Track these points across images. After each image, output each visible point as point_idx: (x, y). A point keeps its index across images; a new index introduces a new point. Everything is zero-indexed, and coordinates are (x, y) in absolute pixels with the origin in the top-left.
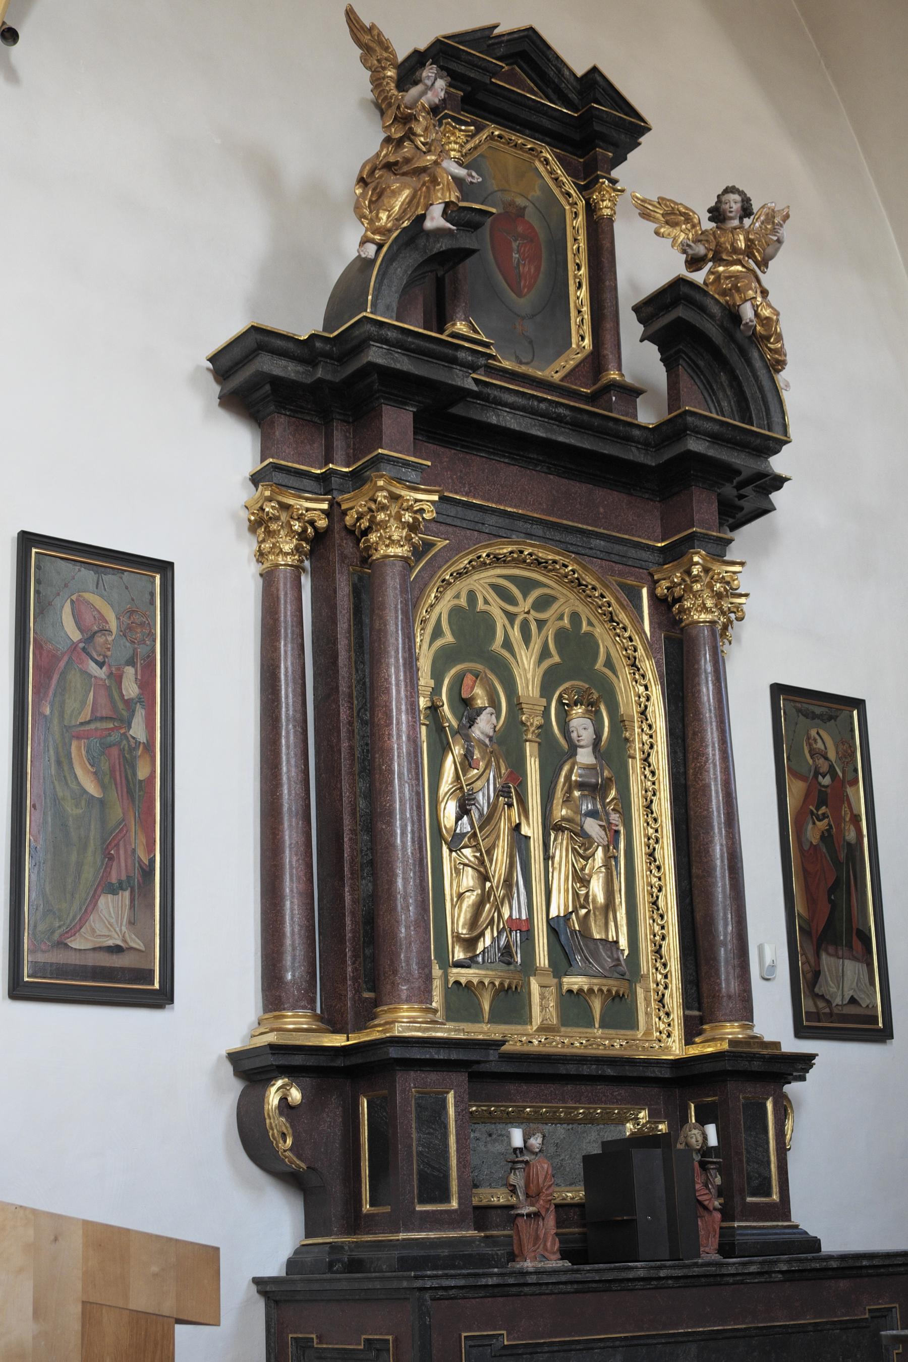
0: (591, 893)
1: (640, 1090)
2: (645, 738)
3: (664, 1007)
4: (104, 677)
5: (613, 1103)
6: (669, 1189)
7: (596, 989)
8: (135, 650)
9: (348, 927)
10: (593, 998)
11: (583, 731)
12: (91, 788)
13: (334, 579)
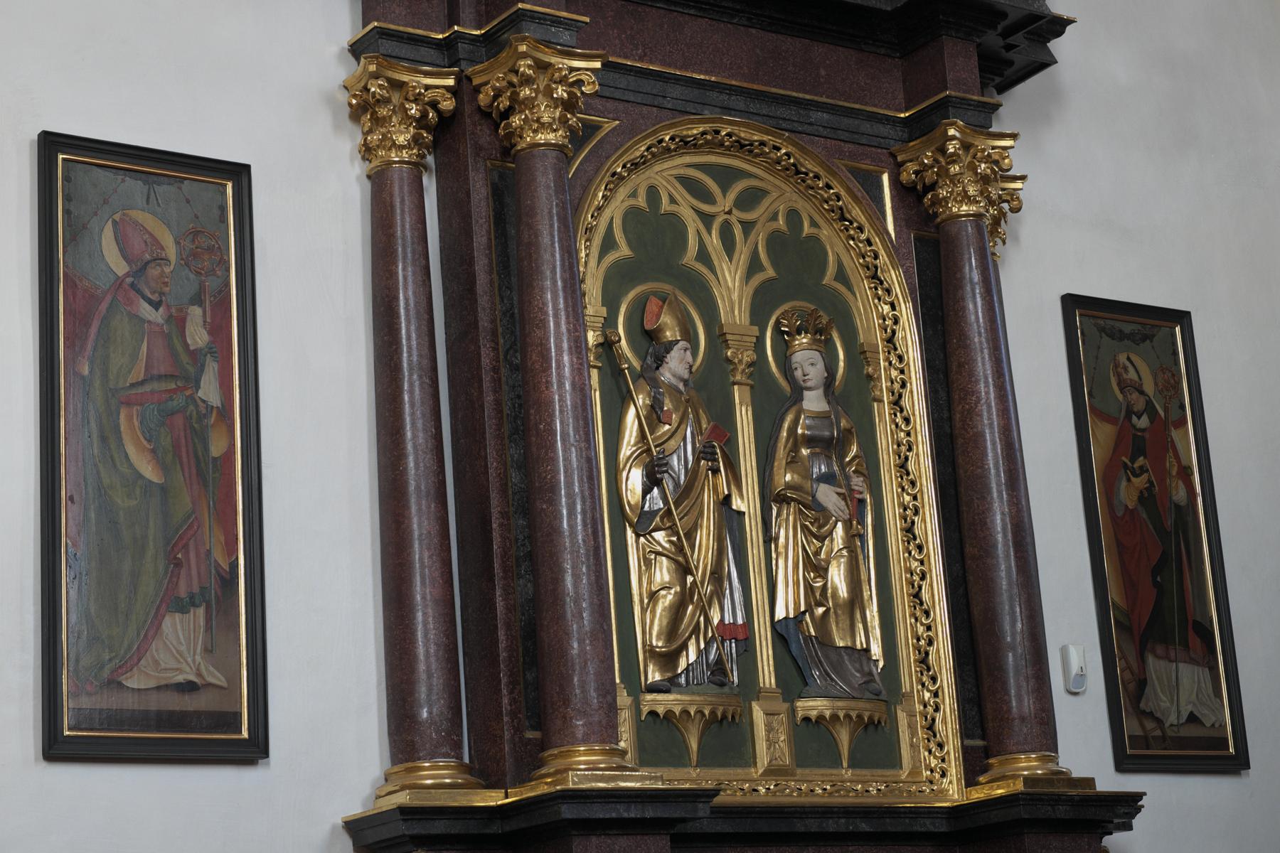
2: (894, 373)
3: (935, 736)
4: (160, 321)
9: (502, 645)
10: (838, 727)
12: (148, 471)
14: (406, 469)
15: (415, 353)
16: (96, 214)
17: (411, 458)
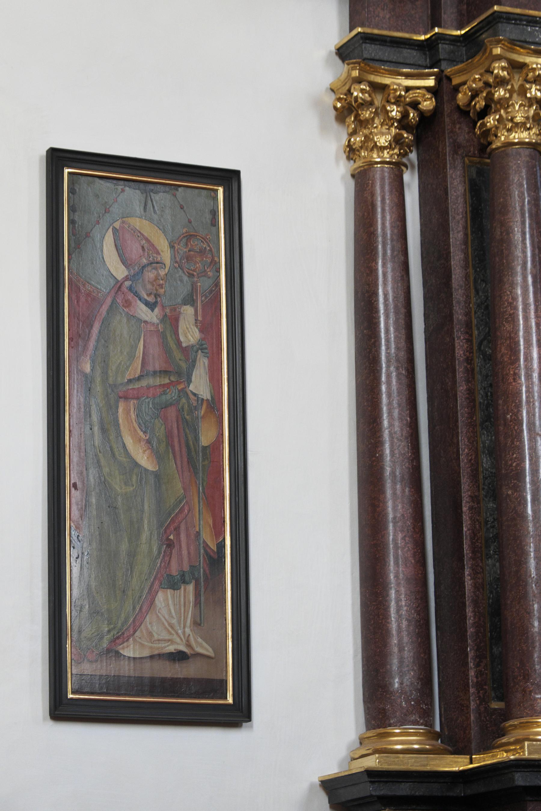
4: (155, 320)
8: (194, 287)
9: (470, 621)
12: (144, 460)
13: (445, 177)
14: (382, 456)
15: (393, 346)
16: (98, 223)
17: (387, 446)
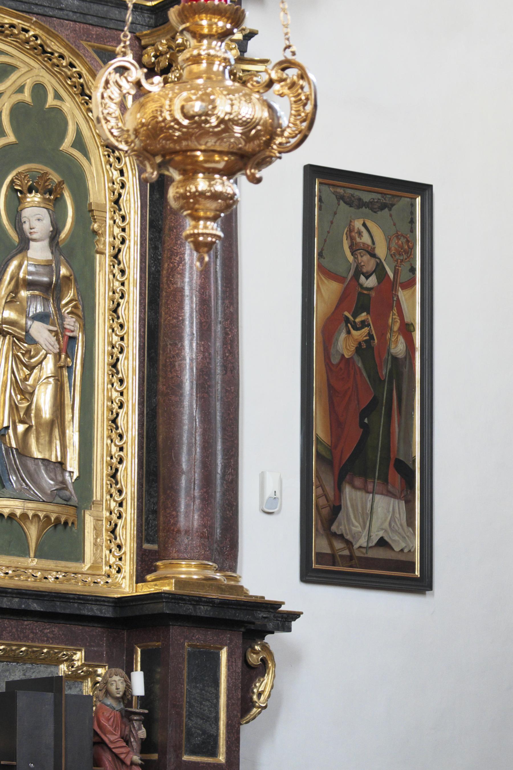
0: (33, 407)
1: (77, 629)
2: (117, 231)
3: (116, 538)
5: (43, 641)
6: (57, 736)
7: (30, 514)
10: (28, 524)
11: (37, 222)
